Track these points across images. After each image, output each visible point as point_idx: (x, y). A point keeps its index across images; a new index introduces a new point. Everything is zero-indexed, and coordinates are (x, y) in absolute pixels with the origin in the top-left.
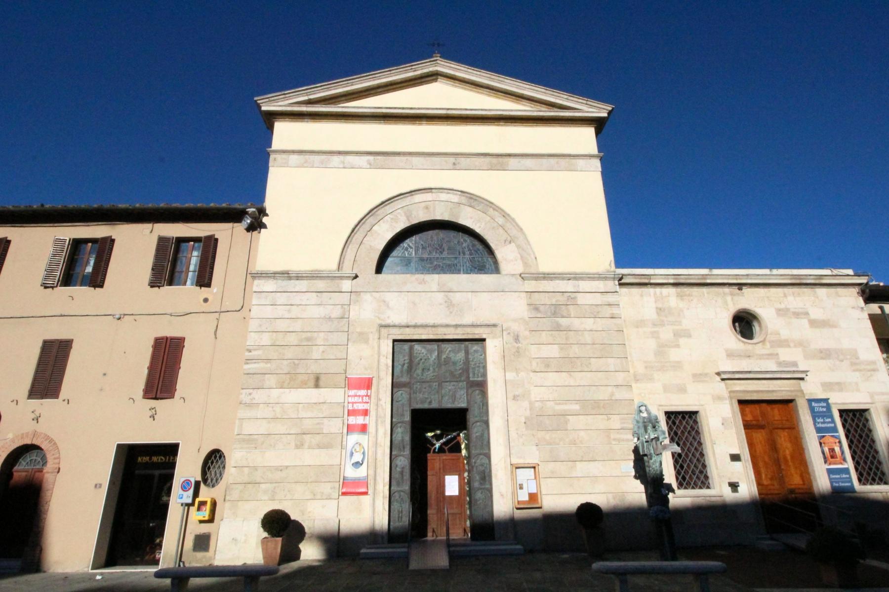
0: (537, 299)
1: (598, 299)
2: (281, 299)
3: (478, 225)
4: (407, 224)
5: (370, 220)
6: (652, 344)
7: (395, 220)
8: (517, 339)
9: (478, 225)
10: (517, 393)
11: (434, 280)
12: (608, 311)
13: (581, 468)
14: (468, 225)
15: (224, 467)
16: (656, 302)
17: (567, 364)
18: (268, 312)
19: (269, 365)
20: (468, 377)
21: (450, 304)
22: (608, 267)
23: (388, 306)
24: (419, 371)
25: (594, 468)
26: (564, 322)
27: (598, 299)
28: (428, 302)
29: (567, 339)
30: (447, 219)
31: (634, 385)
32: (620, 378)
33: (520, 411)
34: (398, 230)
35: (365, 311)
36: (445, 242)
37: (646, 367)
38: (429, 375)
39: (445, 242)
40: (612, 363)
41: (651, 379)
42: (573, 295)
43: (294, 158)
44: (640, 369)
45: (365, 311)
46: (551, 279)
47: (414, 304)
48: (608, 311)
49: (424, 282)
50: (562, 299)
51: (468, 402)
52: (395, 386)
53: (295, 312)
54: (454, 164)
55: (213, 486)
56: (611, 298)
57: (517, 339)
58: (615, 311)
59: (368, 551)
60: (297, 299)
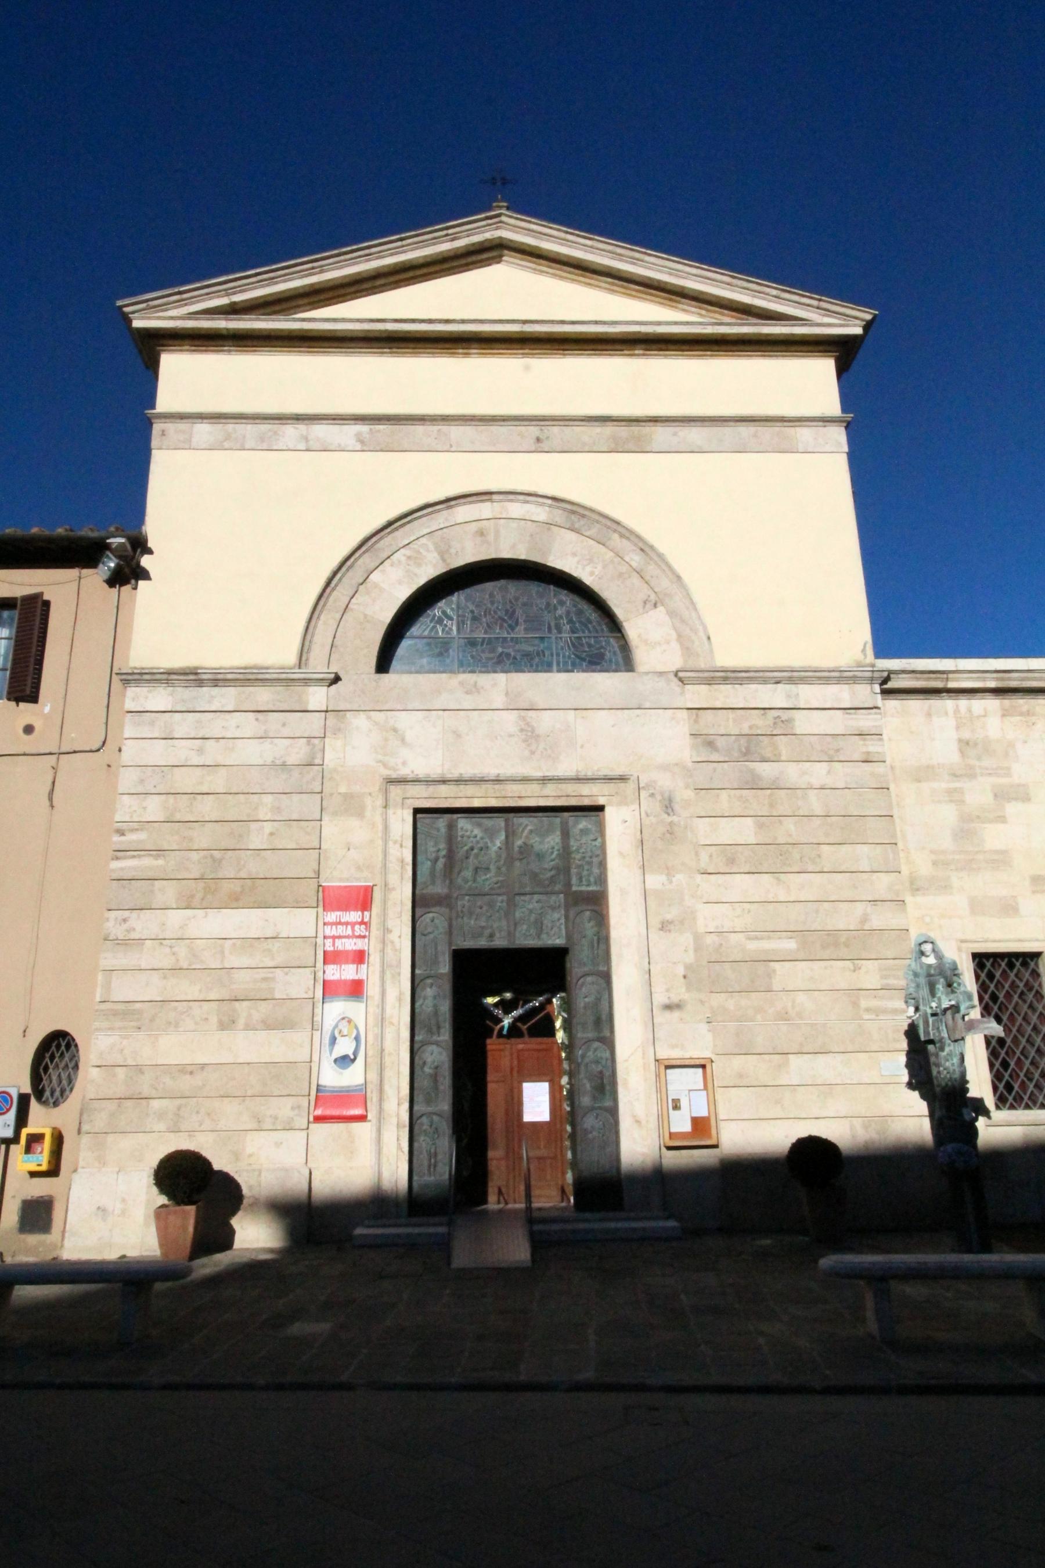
0: (709, 722)
1: (837, 723)
2: (183, 725)
6: (948, 814)
7: (416, 560)
8: (669, 806)
9: (588, 569)
10: (669, 917)
11: (498, 685)
14: (567, 569)
16: (958, 728)
17: (772, 858)
20: (568, 884)
23: (403, 740)
24: (468, 874)
26: (766, 770)
27: (837, 723)
29: (772, 805)
31: (909, 899)
32: (882, 885)
34: (422, 581)
35: (356, 751)
37: (935, 863)
41: (945, 887)
43: (203, 431)
44: (924, 867)
47: (458, 735)
48: (859, 748)
50: (760, 723)
51: (569, 937)
54: (538, 440)
56: (865, 721)
58: (872, 747)
60: (216, 726)
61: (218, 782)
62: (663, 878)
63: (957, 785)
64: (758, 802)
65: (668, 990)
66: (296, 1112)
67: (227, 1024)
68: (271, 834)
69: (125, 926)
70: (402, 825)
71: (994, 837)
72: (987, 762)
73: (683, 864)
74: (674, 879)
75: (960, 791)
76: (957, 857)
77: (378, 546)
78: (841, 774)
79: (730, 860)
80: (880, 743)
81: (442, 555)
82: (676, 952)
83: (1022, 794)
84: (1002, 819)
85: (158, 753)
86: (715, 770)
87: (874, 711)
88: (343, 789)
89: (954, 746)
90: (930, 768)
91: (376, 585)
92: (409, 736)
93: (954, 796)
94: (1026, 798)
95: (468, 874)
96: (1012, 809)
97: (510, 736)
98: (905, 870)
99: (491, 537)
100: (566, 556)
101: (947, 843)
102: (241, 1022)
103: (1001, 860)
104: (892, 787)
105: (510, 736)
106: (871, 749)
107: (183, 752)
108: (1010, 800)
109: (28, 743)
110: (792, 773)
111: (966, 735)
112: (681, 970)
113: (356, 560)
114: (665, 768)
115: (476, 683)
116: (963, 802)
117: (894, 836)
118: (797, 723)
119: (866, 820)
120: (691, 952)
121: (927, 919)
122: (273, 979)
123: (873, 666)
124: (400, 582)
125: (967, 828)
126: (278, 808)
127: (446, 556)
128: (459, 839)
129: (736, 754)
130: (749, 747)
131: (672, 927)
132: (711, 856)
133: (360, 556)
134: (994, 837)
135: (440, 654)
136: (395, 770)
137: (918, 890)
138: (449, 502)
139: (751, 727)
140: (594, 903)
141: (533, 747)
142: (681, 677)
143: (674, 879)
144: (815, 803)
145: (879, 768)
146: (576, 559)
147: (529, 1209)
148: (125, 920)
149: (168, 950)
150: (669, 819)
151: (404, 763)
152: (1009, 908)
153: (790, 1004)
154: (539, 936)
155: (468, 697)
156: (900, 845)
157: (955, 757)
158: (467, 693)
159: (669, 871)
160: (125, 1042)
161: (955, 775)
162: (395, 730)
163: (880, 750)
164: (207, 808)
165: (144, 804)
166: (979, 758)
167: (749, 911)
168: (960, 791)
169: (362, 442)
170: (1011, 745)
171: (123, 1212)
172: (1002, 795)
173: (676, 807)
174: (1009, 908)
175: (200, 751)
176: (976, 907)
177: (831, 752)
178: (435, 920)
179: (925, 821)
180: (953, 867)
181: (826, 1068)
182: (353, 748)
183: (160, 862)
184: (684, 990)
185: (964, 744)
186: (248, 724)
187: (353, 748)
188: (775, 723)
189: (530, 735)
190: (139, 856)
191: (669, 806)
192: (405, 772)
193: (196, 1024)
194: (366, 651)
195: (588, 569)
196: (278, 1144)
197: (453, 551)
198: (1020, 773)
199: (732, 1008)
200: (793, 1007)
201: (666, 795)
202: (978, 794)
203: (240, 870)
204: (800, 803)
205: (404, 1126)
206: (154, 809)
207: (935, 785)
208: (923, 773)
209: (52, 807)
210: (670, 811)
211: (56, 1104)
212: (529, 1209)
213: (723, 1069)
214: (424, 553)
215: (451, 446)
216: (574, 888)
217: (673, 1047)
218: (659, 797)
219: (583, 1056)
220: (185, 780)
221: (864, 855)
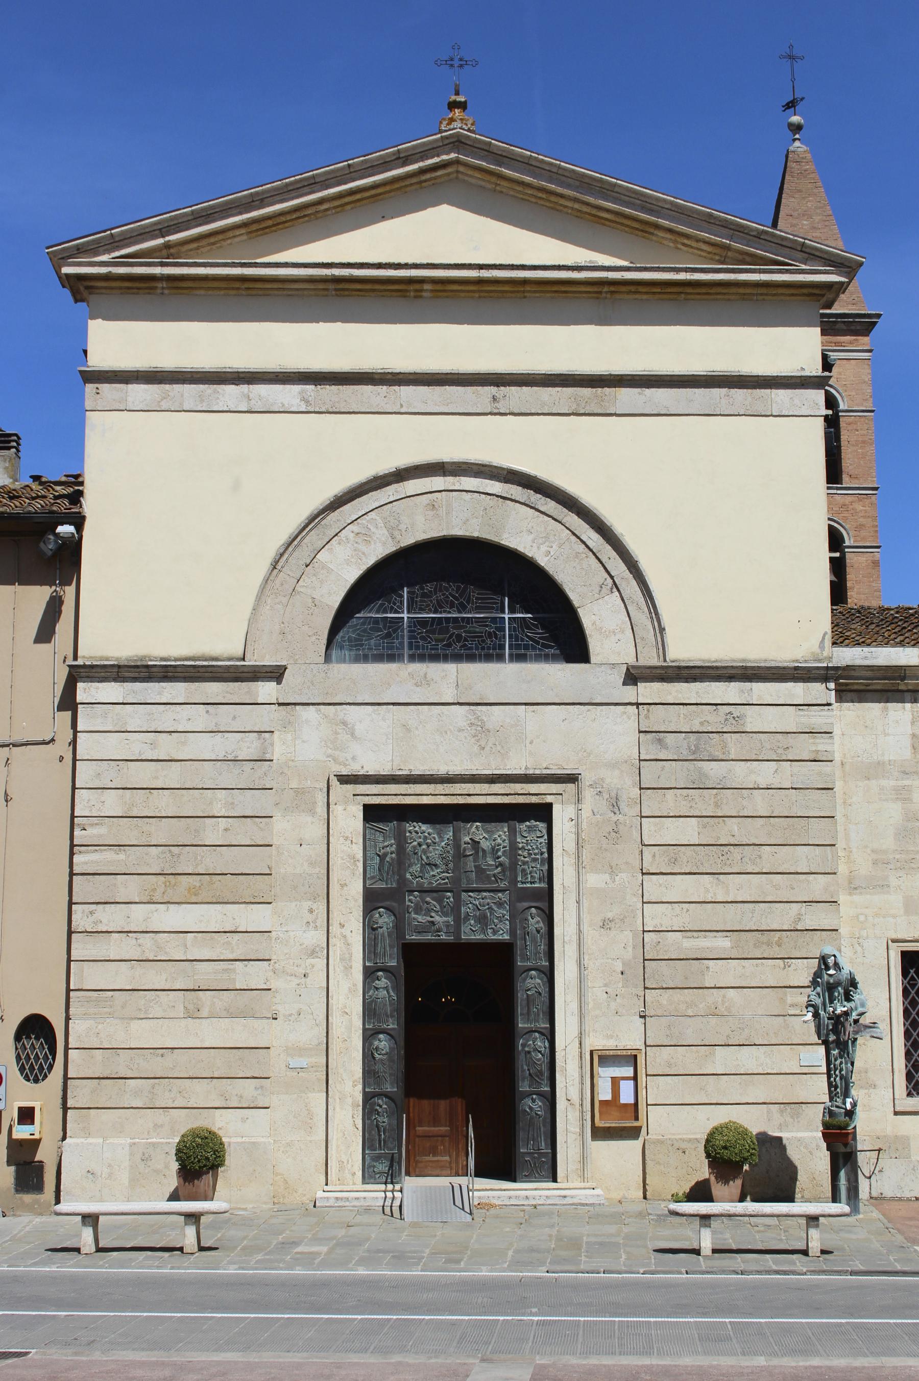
0: (659, 718)
1: (789, 719)
2: (136, 718)
3: (550, 528)
4: (391, 548)
5: (313, 538)
6: (894, 812)
7: (366, 537)
8: (615, 805)
9: (544, 548)
10: (610, 915)
11: (447, 677)
12: (805, 747)
13: (722, 1059)
14: (521, 549)
15: (18, 1058)
16: (913, 723)
17: (717, 856)
18: (113, 746)
19: (122, 856)
20: (514, 881)
21: (481, 730)
22: (816, 649)
23: (353, 734)
24: (416, 868)
25: (749, 1059)
26: (714, 770)
27: (789, 719)
28: (447, 721)
29: (717, 805)
30: (476, 534)
31: (842, 898)
32: (817, 887)
33: (620, 947)
34: (371, 561)
35: (307, 745)
36: (463, 595)
37: (875, 863)
38: (437, 877)
39: (463, 595)
40: (803, 858)
41: (882, 886)
42: (736, 711)
43: (139, 392)
44: (864, 867)
45: (307, 745)
46: (694, 679)
47: (406, 728)
48: (805, 747)
49: (425, 681)
50: (713, 719)
51: (512, 932)
52: (372, 900)
53: (166, 747)
54: (494, 399)
55: (36, 1081)
56: (816, 719)
57: (615, 805)
58: (821, 745)
59: (356, 1317)
60: (166, 718)
63: (906, 782)
65: (606, 985)
66: (259, 1091)
68: (226, 830)
69: (91, 919)
70: (349, 820)
73: (627, 863)
74: (617, 878)
75: (908, 789)
76: (898, 856)
77: (322, 523)
80: (830, 741)
81: (392, 531)
86: (663, 768)
87: (826, 707)
91: (324, 567)
92: (359, 728)
97: (460, 730)
98: (842, 869)
99: (442, 512)
101: (888, 842)
102: (205, 1012)
104: (839, 786)
105: (460, 730)
106: (821, 747)
107: (137, 746)
110: (741, 773)
112: (619, 967)
113: (304, 538)
115: (426, 674)
117: (835, 837)
118: (749, 720)
120: (630, 949)
121: (862, 918)
122: (234, 970)
124: (348, 562)
126: (233, 803)
127: (396, 533)
128: (408, 834)
129: (685, 753)
130: (700, 745)
131: (612, 925)
132: (654, 856)
133: (307, 534)
135: (388, 635)
136: (345, 765)
137: (855, 888)
139: (702, 723)
141: (483, 743)
143: (617, 878)
146: (531, 537)
148: (91, 913)
149: (134, 941)
150: (615, 818)
151: (354, 758)
153: (720, 1000)
154: (484, 931)
155: (418, 689)
156: (841, 845)
158: (417, 685)
160: (100, 1026)
161: (905, 773)
162: (344, 723)
163: (828, 748)
165: (103, 799)
167: (688, 910)
168: (908, 789)
169: (308, 402)
171: (110, 1175)
173: (622, 805)
177: (780, 751)
178: (384, 920)
180: (890, 866)
182: (303, 742)
184: (620, 985)
186: (199, 718)
187: (303, 742)
188: (726, 720)
190: (101, 851)
193: (164, 1011)
194: (314, 638)
196: (244, 1120)
197: (403, 527)
199: (665, 1002)
200: (723, 1002)
201: (613, 794)
203: (197, 865)
204: (745, 803)
205: (359, 1106)
207: (884, 782)
209: (217, 1249)
210: (616, 810)
213: (656, 1060)
214: (373, 529)
215: (402, 406)
216: (520, 885)
218: (606, 796)
219: (524, 1045)
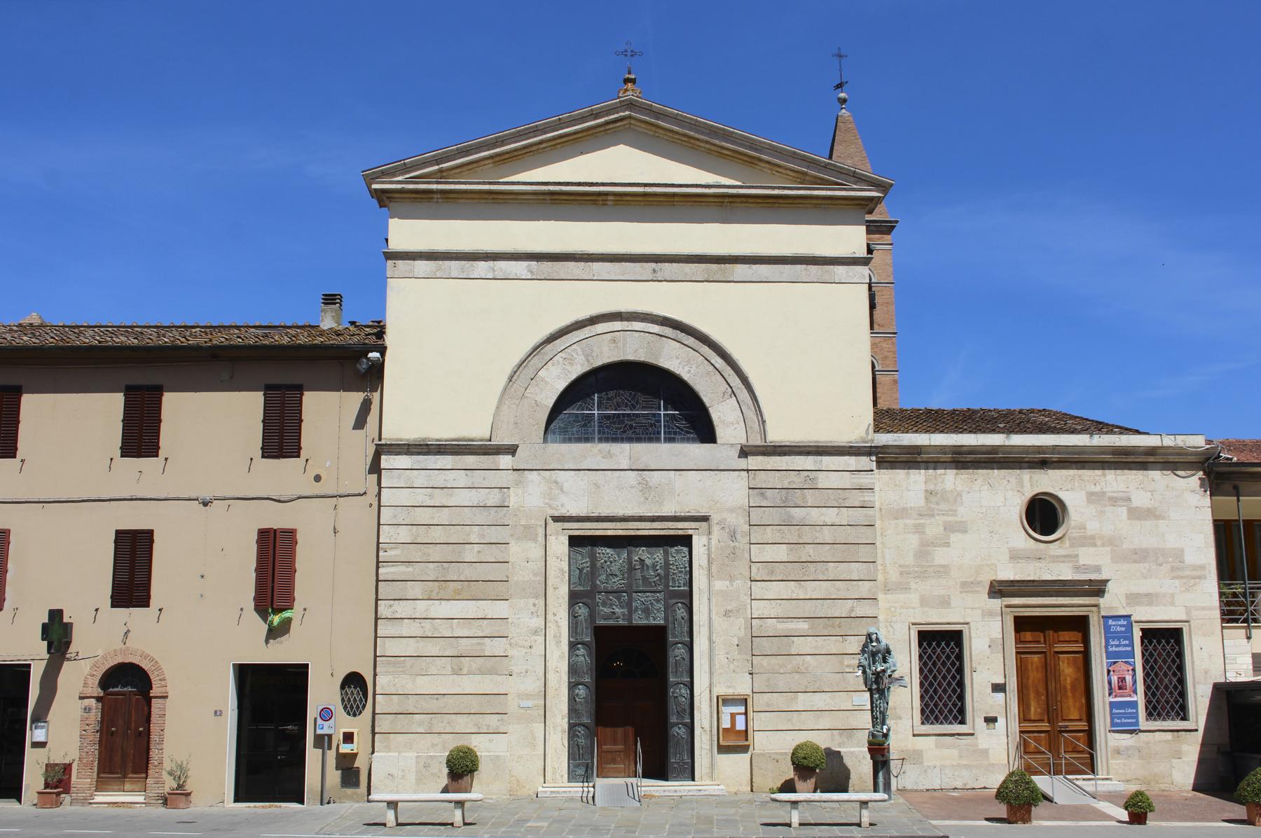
0: (762, 480)
2: (420, 479)
6: (914, 540)
8: (733, 536)
9: (687, 369)
14: (672, 369)
20: (667, 586)
24: (603, 577)
26: (797, 513)
27: (846, 480)
29: (799, 536)
31: (880, 597)
32: (864, 589)
34: (574, 376)
37: (901, 574)
41: (906, 589)
43: (422, 266)
44: (894, 576)
50: (797, 480)
51: (666, 619)
56: (864, 480)
58: (867, 497)
61: (443, 516)
62: (727, 583)
64: (791, 534)
67: (457, 672)
71: (940, 556)
72: (943, 506)
78: (845, 516)
79: (772, 572)
81: (587, 357)
82: (736, 629)
83: (961, 528)
84: (947, 545)
85: (405, 497)
88: (523, 523)
89: (922, 495)
90: (904, 509)
91: (543, 380)
92: (566, 486)
93: (919, 529)
94: (965, 531)
95: (603, 577)
96: (954, 538)
98: (880, 577)
99: (620, 344)
100: (676, 358)
101: (910, 560)
103: (943, 571)
104: (878, 524)
107: (420, 497)
108: (953, 532)
109: (318, 489)
110: (815, 515)
111: (931, 487)
114: (731, 510)
116: (924, 533)
117: (876, 556)
119: (857, 547)
123: (872, 441)
125: (923, 552)
130: (789, 496)
134: (940, 556)
138: (593, 320)
140: (687, 598)
142: (744, 452)
144: (827, 535)
145: (869, 512)
147: (1238, 496)
152: (945, 602)
156: (879, 562)
157: (922, 503)
159: (732, 579)
162: (556, 482)
164: (437, 534)
166: (937, 504)
168: (923, 525)
169: (532, 273)
170: (959, 495)
172: (950, 528)
173: (738, 536)
174: (945, 602)
175: (431, 496)
176: (924, 602)
178: (582, 611)
179: (895, 546)
181: (819, 701)
183: (410, 569)
185: (930, 494)
186: (461, 478)
189: (646, 487)
191: (733, 536)
192: (563, 512)
195: (687, 369)
198: (963, 513)
202: (934, 528)
206: (404, 534)
207: (907, 521)
208: (901, 513)
211: (355, 715)
212: (1238, 496)
213: (759, 702)
217: (729, 687)
220: (423, 516)
221: (855, 570)
